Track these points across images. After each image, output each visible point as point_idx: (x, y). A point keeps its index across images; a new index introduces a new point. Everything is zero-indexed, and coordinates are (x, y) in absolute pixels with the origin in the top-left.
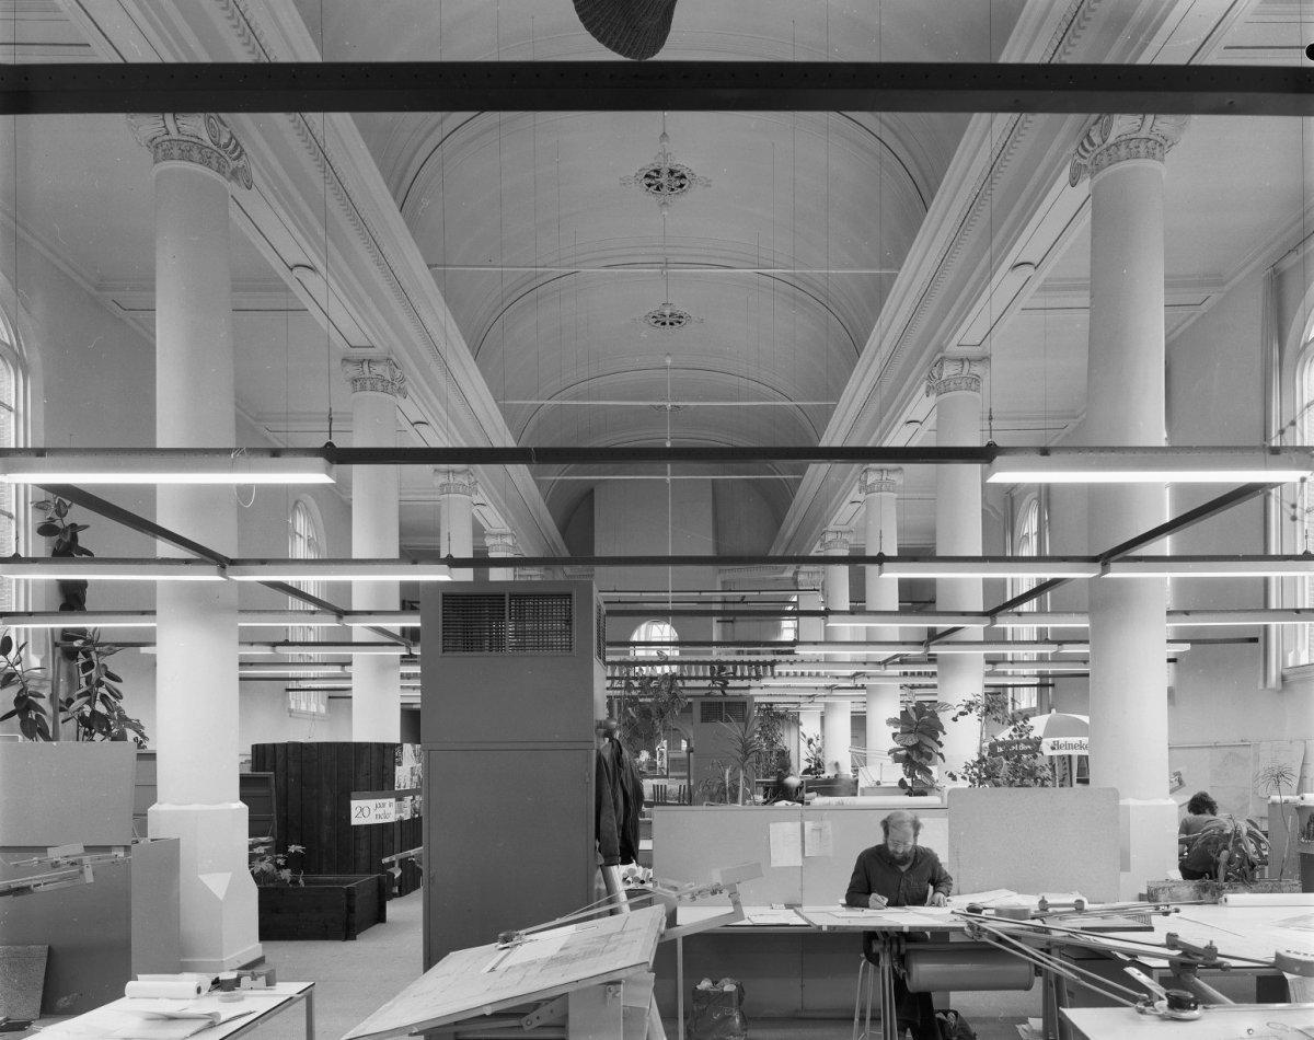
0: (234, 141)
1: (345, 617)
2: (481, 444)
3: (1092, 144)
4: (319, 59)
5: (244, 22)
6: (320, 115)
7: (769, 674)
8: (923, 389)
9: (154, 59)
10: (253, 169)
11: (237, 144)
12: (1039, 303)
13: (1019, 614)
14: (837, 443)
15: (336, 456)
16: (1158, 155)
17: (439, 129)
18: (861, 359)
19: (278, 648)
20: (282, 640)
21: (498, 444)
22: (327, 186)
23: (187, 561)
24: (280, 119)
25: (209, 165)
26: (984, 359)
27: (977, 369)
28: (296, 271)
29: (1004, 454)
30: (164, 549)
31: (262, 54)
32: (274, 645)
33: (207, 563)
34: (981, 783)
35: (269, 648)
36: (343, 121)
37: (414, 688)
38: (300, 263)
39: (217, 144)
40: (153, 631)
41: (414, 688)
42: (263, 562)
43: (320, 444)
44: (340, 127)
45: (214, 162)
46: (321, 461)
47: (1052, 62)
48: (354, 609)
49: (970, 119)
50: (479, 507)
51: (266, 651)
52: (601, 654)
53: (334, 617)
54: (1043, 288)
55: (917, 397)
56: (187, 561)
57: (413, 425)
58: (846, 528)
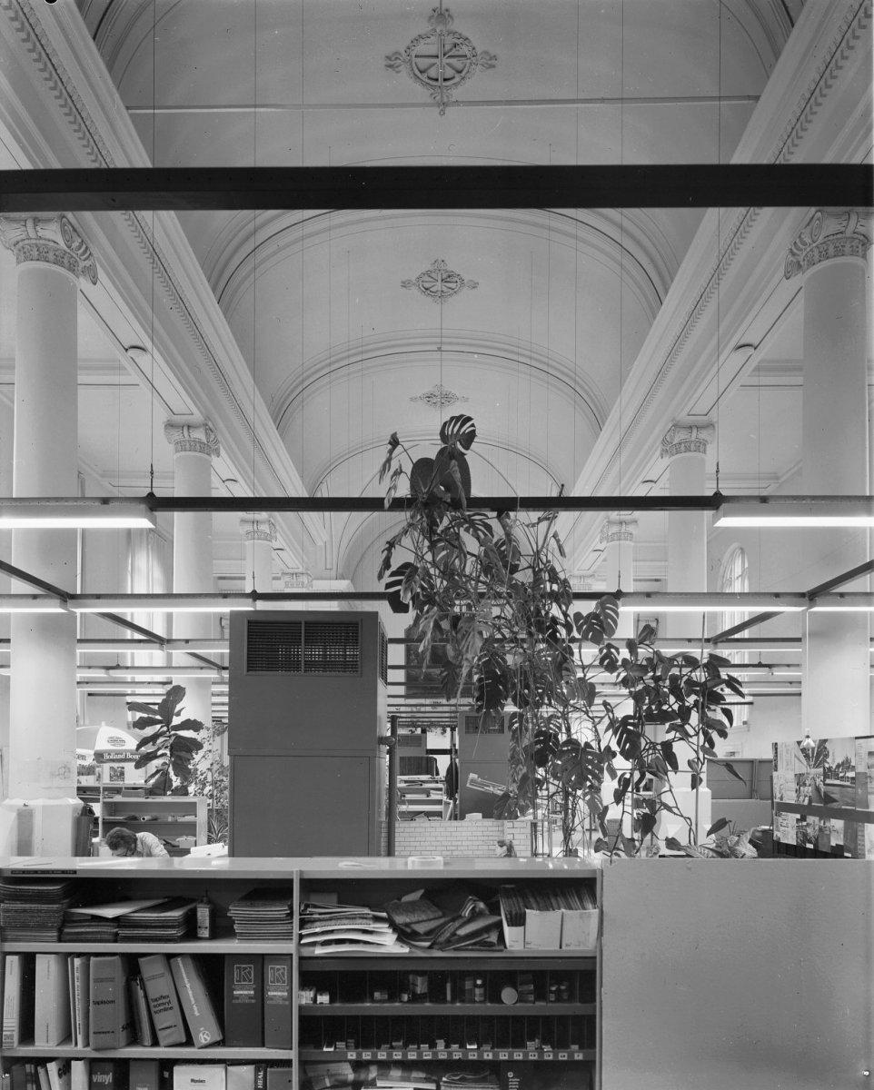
0: (84, 246)
1: (69, 601)
2: (278, 494)
3: (805, 244)
4: (149, 165)
5: (57, 77)
6: (151, 212)
7: (860, 253)
8: (658, 453)
9: (16, 167)
10: (98, 266)
11: (87, 248)
12: (754, 381)
13: (842, 595)
14: (586, 494)
15: (155, 504)
16: (860, 253)
17: (252, 239)
18: (652, 330)
19: (111, 671)
20: (114, 665)
21: (293, 494)
22: (156, 275)
23: (35, 597)
24: (117, 217)
25: (62, 265)
26: (710, 426)
27: (704, 435)
28: (227, 483)
29: (728, 502)
30: (129, 634)
31: (103, 162)
32: (108, 668)
33: (51, 597)
34: (82, 791)
35: (103, 671)
36: (169, 217)
37: (223, 704)
38: (134, 344)
39: (69, 247)
40: (7, 656)
41: (223, 704)
42: (98, 597)
43: (144, 493)
44: (164, 224)
45: (66, 261)
46: (143, 507)
47: (777, 162)
48: (174, 638)
49: (704, 215)
50: (279, 552)
51: (101, 674)
52: (384, 677)
53: (58, 601)
54: (758, 369)
55: (654, 458)
56: (35, 597)
57: (127, 350)
58: (590, 572)
